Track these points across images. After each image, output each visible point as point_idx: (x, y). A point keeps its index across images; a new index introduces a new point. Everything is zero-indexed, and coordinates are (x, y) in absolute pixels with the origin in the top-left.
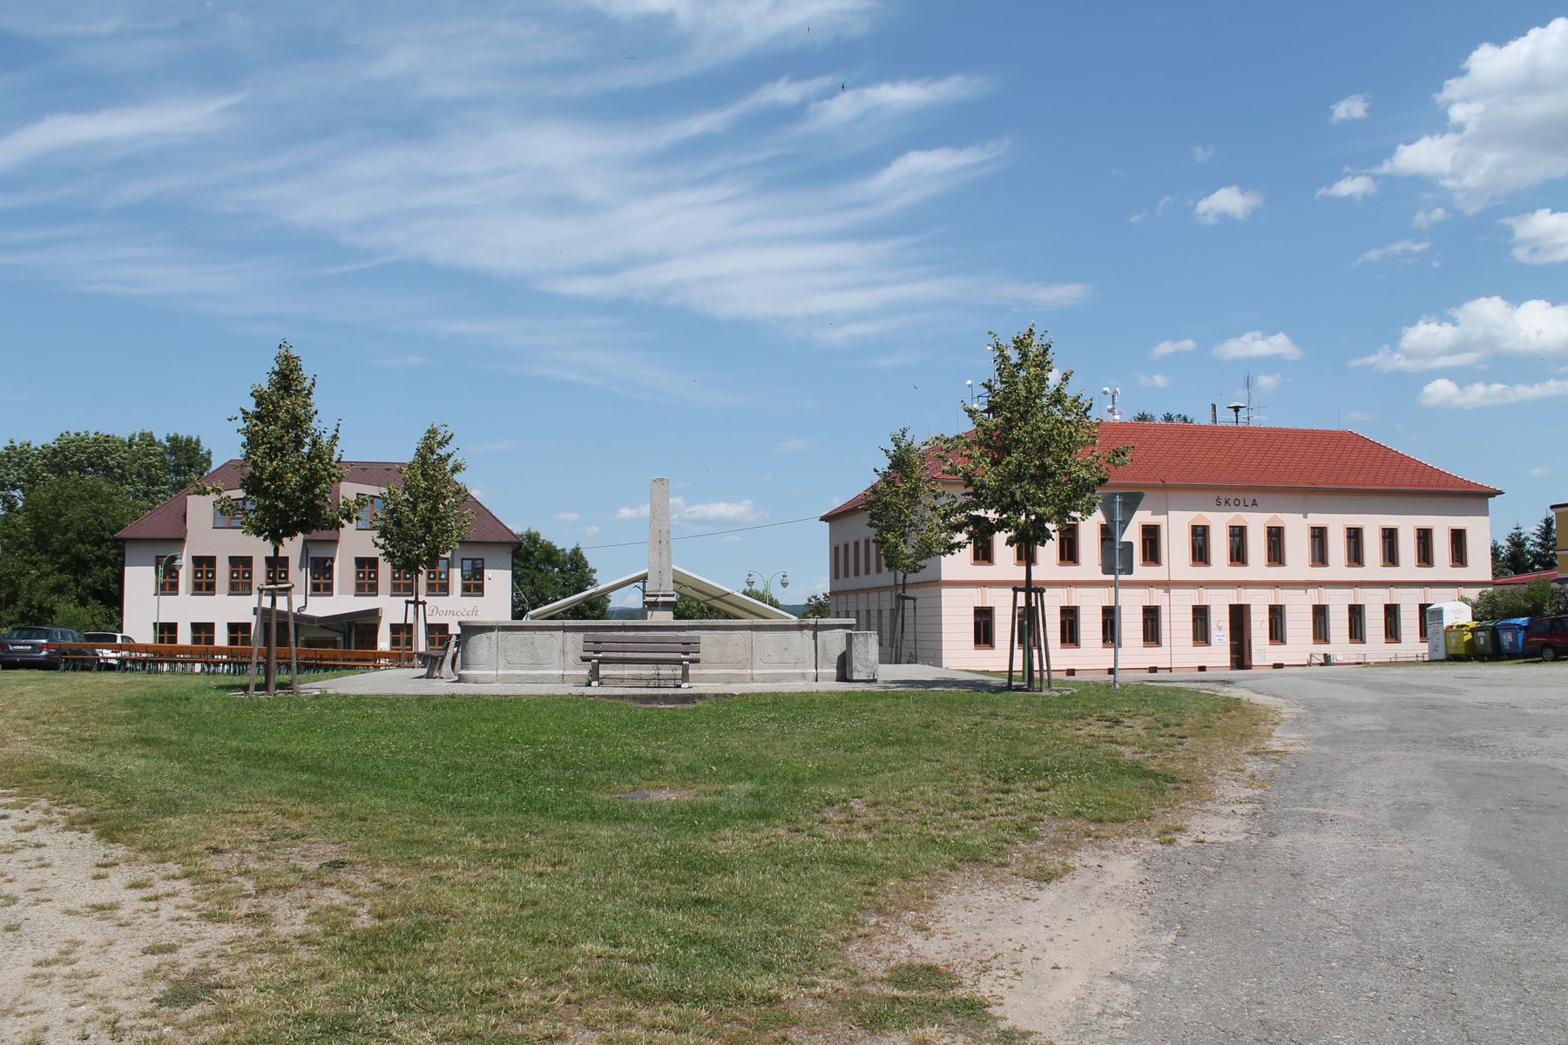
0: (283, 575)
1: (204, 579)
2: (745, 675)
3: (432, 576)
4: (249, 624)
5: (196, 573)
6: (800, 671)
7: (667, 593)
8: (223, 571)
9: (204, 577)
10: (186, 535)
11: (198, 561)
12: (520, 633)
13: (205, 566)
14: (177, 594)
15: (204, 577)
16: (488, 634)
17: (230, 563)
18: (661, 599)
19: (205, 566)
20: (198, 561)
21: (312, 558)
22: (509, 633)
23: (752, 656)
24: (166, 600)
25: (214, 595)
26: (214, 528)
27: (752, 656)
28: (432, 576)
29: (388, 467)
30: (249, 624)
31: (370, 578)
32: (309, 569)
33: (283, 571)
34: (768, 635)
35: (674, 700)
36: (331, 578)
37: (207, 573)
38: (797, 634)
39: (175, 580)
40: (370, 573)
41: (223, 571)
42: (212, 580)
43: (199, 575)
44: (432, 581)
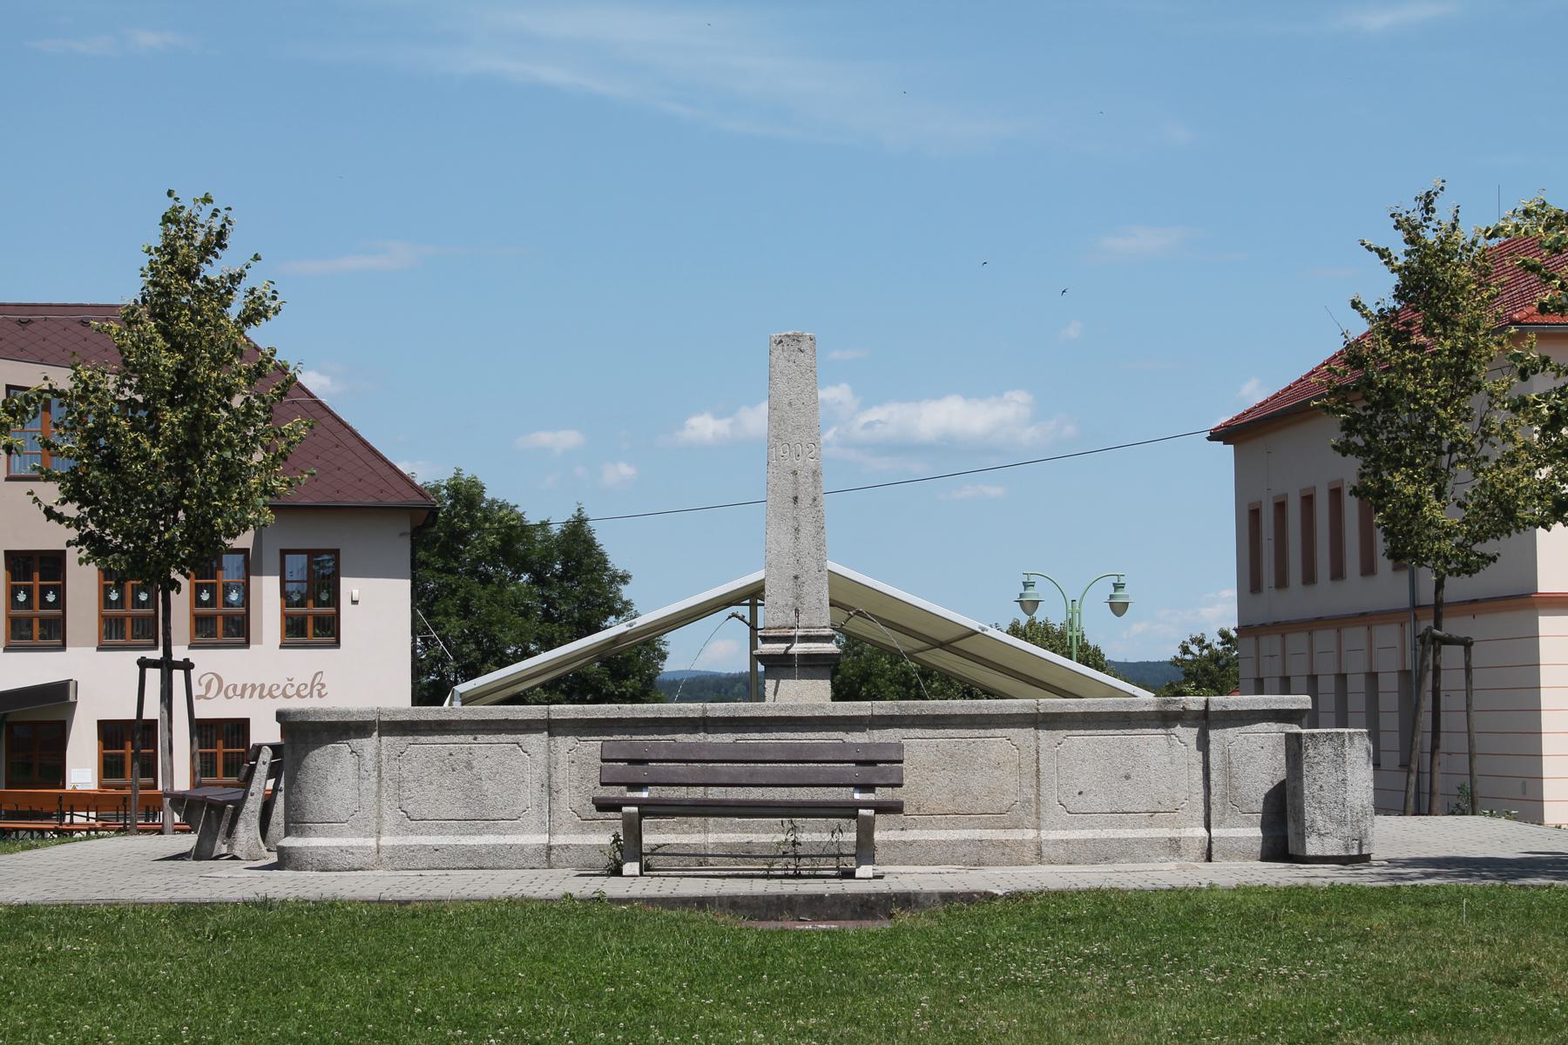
2: (1022, 843)
6: (1166, 833)
7: (813, 632)
12: (437, 738)
13: (37, 575)
18: (798, 648)
19: (37, 575)
22: (410, 739)
25: (63, 647)
26: (8, 479)
28: (205, 597)
31: (44, 604)
34: (1079, 741)
40: (44, 591)
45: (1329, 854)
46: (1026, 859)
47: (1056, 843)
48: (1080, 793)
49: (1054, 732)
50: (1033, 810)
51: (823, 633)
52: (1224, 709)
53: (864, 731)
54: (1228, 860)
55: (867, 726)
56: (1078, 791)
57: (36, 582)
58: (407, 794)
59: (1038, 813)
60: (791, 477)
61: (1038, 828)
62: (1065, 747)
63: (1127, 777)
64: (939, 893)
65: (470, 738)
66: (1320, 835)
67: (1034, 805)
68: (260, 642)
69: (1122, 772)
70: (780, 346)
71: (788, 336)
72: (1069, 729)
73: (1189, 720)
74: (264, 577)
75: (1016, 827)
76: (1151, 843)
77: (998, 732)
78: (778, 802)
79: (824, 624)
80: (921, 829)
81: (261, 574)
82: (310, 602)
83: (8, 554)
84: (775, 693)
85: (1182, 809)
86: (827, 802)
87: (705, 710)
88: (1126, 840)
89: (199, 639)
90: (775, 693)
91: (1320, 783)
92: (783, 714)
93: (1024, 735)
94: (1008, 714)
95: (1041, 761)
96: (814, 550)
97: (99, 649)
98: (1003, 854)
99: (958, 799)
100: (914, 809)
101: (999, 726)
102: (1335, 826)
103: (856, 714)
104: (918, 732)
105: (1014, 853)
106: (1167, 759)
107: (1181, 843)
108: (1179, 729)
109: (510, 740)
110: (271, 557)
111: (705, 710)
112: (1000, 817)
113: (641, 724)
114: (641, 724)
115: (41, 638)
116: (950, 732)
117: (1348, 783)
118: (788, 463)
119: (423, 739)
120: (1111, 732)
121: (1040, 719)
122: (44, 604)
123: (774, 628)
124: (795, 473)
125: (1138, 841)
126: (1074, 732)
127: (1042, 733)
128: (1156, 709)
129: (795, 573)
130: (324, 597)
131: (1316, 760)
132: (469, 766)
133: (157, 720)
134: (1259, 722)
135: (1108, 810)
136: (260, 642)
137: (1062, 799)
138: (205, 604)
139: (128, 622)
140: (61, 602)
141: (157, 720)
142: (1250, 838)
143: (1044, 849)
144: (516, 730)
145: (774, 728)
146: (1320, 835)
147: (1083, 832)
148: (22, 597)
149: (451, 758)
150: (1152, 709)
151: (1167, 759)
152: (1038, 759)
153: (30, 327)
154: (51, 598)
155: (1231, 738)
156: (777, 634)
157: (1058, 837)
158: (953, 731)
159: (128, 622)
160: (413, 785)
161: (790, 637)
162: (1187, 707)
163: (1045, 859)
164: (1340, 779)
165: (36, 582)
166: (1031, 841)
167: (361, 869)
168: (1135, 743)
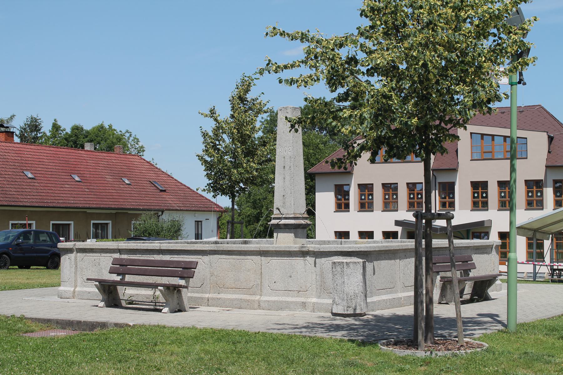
0: (484, 195)
1: (535, 198)
2: (254, 301)
3: (476, 195)
4: (397, 232)
5: (361, 195)
6: (302, 300)
7: (288, 216)
8: (378, 194)
9: (391, 198)
10: (458, 166)
11: (362, 187)
12: (91, 254)
13: (480, 188)
14: (349, 211)
15: (391, 198)
16: (69, 255)
17: (526, 185)
18: (283, 222)
19: (480, 188)
20: (362, 187)
21: (439, 183)
22: (84, 254)
23: (261, 282)
24: (342, 215)
25: (487, 210)
26: (471, 160)
27: (261, 282)
28: (530, 194)
29: (503, 111)
30: (397, 232)
31: (482, 197)
32: (437, 191)
33: (503, 192)
34: (275, 261)
35: (85, 327)
36: (454, 197)
37: (537, 193)
38: (299, 262)
39: (453, 200)
40: (482, 193)
41: (378, 194)
42: (541, 198)
43: (363, 197)
44: (503, 199)
45: (339, 312)
46: (255, 307)
47: (265, 301)
48: (275, 282)
49: (267, 258)
50: (260, 288)
51: (290, 216)
52: (319, 250)
53: (208, 256)
54: (320, 312)
55: (208, 254)
56: (274, 281)
57: (480, 190)
58: (84, 273)
59: (261, 289)
60: (283, 159)
61: (261, 295)
62: (270, 264)
63: (291, 277)
64: (114, 323)
65: (99, 254)
66: (336, 304)
67: (260, 286)
68: (547, 208)
69: (289, 275)
70: (281, 112)
71: (283, 107)
72: (272, 257)
73: (312, 254)
74: (548, 189)
75: (254, 295)
76: (296, 303)
77: (249, 257)
78: (136, 282)
79: (292, 213)
80: (224, 293)
81: (546, 187)
82: (447, 197)
83: (471, 182)
84: (277, 238)
85: (309, 290)
86: (149, 283)
87: (160, 247)
88: (288, 302)
89: (501, 208)
90: (277, 238)
91: (336, 283)
92: (182, 249)
93: (257, 258)
94: (251, 251)
95: (262, 269)
96: (289, 186)
97: (498, 210)
98: (248, 305)
99: (236, 283)
100: (222, 286)
101: (249, 255)
102: (341, 301)
103: (204, 249)
104: (224, 256)
105: (251, 304)
106: (304, 270)
107: (306, 304)
108: (308, 258)
109: (109, 256)
110: (550, 182)
111: (160, 247)
112: (248, 290)
113: (144, 251)
114: (144, 251)
115: (482, 207)
116: (234, 257)
117: (346, 283)
118: (282, 154)
119: (88, 254)
120: (285, 258)
121: (262, 253)
122: (537, 196)
123: (277, 214)
124: (284, 158)
125: (292, 302)
126: (273, 258)
127: (263, 258)
128: (298, 250)
129: (283, 194)
130: (451, 196)
131: (336, 273)
132: (99, 265)
133: (373, 239)
134: (334, 256)
135: (284, 290)
136: (547, 208)
137: (269, 284)
138: (503, 197)
139: (535, 202)
140: (487, 197)
141: (373, 239)
142: (328, 304)
143: (261, 303)
144: (111, 252)
145: (182, 254)
146: (336, 304)
147: (275, 298)
148: (412, 196)
149: (95, 261)
150: (297, 250)
151: (304, 270)
152: (261, 268)
153: (523, 113)
154: (539, 194)
155: (323, 262)
156: (277, 217)
157: (266, 299)
158: (235, 256)
159: (535, 202)
160: (86, 270)
161: (280, 218)
162: (309, 249)
163: (261, 308)
164: (343, 281)
165: (480, 190)
166: (257, 300)
167: (69, 298)
168: (293, 263)
